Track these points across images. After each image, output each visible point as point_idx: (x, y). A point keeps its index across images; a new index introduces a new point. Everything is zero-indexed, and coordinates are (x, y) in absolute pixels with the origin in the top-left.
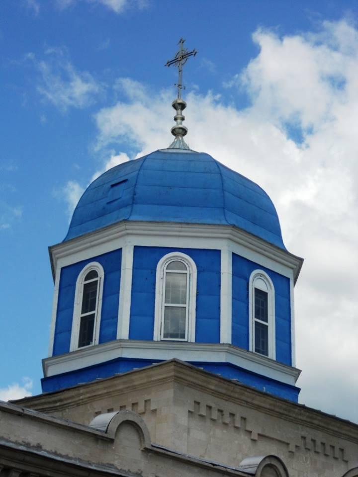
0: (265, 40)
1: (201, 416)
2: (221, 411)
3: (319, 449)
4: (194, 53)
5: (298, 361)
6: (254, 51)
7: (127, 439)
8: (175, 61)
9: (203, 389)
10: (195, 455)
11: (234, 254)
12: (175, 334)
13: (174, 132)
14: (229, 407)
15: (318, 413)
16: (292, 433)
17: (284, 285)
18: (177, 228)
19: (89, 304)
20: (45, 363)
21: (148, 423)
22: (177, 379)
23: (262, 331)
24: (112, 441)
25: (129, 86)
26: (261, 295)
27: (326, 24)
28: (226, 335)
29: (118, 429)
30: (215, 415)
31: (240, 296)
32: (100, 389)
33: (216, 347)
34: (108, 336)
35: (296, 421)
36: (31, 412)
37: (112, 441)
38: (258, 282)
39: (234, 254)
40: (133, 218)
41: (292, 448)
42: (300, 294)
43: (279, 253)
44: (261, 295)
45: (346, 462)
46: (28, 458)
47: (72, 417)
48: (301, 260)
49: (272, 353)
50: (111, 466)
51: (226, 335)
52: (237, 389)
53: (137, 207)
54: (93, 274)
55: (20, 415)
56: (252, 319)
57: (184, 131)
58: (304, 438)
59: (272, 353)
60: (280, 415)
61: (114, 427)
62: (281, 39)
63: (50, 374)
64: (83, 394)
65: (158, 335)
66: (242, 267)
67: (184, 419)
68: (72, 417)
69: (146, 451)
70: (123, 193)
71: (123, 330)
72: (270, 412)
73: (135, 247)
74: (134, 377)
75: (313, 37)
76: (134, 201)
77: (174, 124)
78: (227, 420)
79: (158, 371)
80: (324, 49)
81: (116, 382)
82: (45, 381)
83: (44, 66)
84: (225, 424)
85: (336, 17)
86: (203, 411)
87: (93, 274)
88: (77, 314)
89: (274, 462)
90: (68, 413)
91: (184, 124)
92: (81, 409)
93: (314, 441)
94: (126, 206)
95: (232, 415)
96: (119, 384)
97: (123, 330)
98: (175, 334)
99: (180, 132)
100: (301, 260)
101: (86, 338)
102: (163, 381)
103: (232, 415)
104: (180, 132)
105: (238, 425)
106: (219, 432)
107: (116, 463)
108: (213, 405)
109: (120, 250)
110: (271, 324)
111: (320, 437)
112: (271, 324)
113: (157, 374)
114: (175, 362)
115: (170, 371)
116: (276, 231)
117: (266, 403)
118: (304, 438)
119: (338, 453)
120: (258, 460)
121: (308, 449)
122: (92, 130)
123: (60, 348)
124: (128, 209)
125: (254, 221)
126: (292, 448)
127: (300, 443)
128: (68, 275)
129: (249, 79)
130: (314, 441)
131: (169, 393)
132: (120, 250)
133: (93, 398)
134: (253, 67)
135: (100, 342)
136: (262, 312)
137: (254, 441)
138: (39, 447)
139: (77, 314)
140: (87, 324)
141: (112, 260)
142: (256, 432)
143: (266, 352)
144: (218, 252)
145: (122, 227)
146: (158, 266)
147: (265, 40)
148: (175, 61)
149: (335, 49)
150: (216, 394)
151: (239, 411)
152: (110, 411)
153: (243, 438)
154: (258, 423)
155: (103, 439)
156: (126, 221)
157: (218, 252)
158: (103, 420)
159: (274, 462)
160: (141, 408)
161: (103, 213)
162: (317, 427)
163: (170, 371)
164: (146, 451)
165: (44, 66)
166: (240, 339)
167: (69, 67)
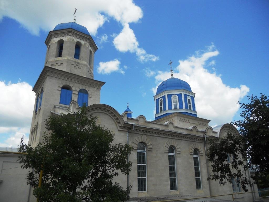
0: (180, 62)
1: (182, 121)
2: (185, 120)
3: (202, 124)
4: (173, 62)
5: (196, 111)
6: (179, 64)
7: (171, 125)
8: (170, 64)
9: (181, 116)
10: (182, 127)
11: (184, 94)
12: (176, 107)
13: (171, 75)
14: (186, 119)
15: (201, 118)
16: (197, 122)
17: (193, 98)
18: (174, 91)
19: (161, 105)
20: (155, 115)
21: (174, 123)
22: (177, 115)
23: (190, 106)
24: (168, 126)
25: (160, 72)
26: (189, 100)
27: (190, 58)
28: (184, 107)
29: (169, 124)
30: (184, 120)
31: (186, 101)
32: (165, 118)
33: (183, 109)
34: (165, 110)
35: (197, 120)
36: (155, 123)
37: (168, 126)
38: (188, 98)
39: (184, 94)
40: (167, 90)
41: (197, 124)
42: (195, 98)
43: (191, 93)
44: (189, 100)
45: (206, 126)
46: (156, 130)
47: (161, 123)
48: (195, 93)
49: (192, 109)
50: (168, 130)
51: (184, 107)
52: (187, 116)
53: (167, 88)
54: (161, 100)
55: (153, 123)
56: (188, 104)
57: (173, 75)
58: (199, 123)
59: (192, 109)
60: (194, 119)
61: (168, 124)
62: (183, 61)
63: (156, 117)
64: (162, 119)
65: (173, 108)
66: (186, 96)
67: (179, 122)
68: (161, 123)
69: (174, 127)
70: (164, 86)
71: (167, 108)
72: (193, 119)
73: (168, 95)
74: (170, 116)
75: (188, 60)
76: (166, 87)
77: (171, 74)
78: (186, 121)
79: (174, 114)
80: (190, 62)
81: (167, 117)
82: (156, 118)
83: (146, 71)
84: (186, 122)
85: (191, 56)
86: (182, 120)
87: (161, 100)
88: (160, 107)
89: (195, 127)
90: (160, 122)
91: (173, 74)
92: (162, 122)
93: (201, 123)
94: (165, 88)
95: (187, 120)
96: (168, 117)
97: (167, 108)
98: (176, 107)
99: (172, 75)
100: (195, 93)
101: (161, 110)
102: (174, 116)
103: (187, 120)
104: (172, 75)
105: (188, 122)
106: (185, 123)
107: (169, 129)
108: (184, 119)
109: (165, 95)
110: (191, 105)
111: (201, 122)
112: (191, 105)
113: (175, 114)
114: (176, 112)
115: (176, 114)
116: (190, 89)
117: (192, 118)
118: (199, 123)
119: (205, 125)
120: (192, 127)
121: (200, 125)
122: (155, 80)
123: (157, 112)
124: (166, 89)
125: (186, 88)
126: (197, 124)
127: (198, 124)
128: (157, 101)
129: (179, 68)
130: (201, 123)
131: (176, 118)
132: (165, 95)
133: (164, 120)
134: (179, 66)
135: (164, 111)
136: (190, 103)
137: (190, 124)
138: (157, 128)
139: (160, 107)
140: (161, 108)
141: (164, 97)
142: (191, 122)
143: (191, 110)
144: (181, 94)
145: (165, 92)
146: (172, 97)
147: (180, 62)
148: (170, 64)
149: (192, 61)
150: (184, 117)
151: (188, 119)
152: (167, 121)
153: (189, 123)
154: (191, 121)
155: (167, 126)
156: (165, 91)
157: (181, 94)
158: (166, 123)
159: (195, 127)
160: (172, 120)
161: (161, 90)
162: (201, 121)
163: (176, 114)
164: (174, 127)
165: (146, 71)
166: (186, 108)
167: (150, 71)
